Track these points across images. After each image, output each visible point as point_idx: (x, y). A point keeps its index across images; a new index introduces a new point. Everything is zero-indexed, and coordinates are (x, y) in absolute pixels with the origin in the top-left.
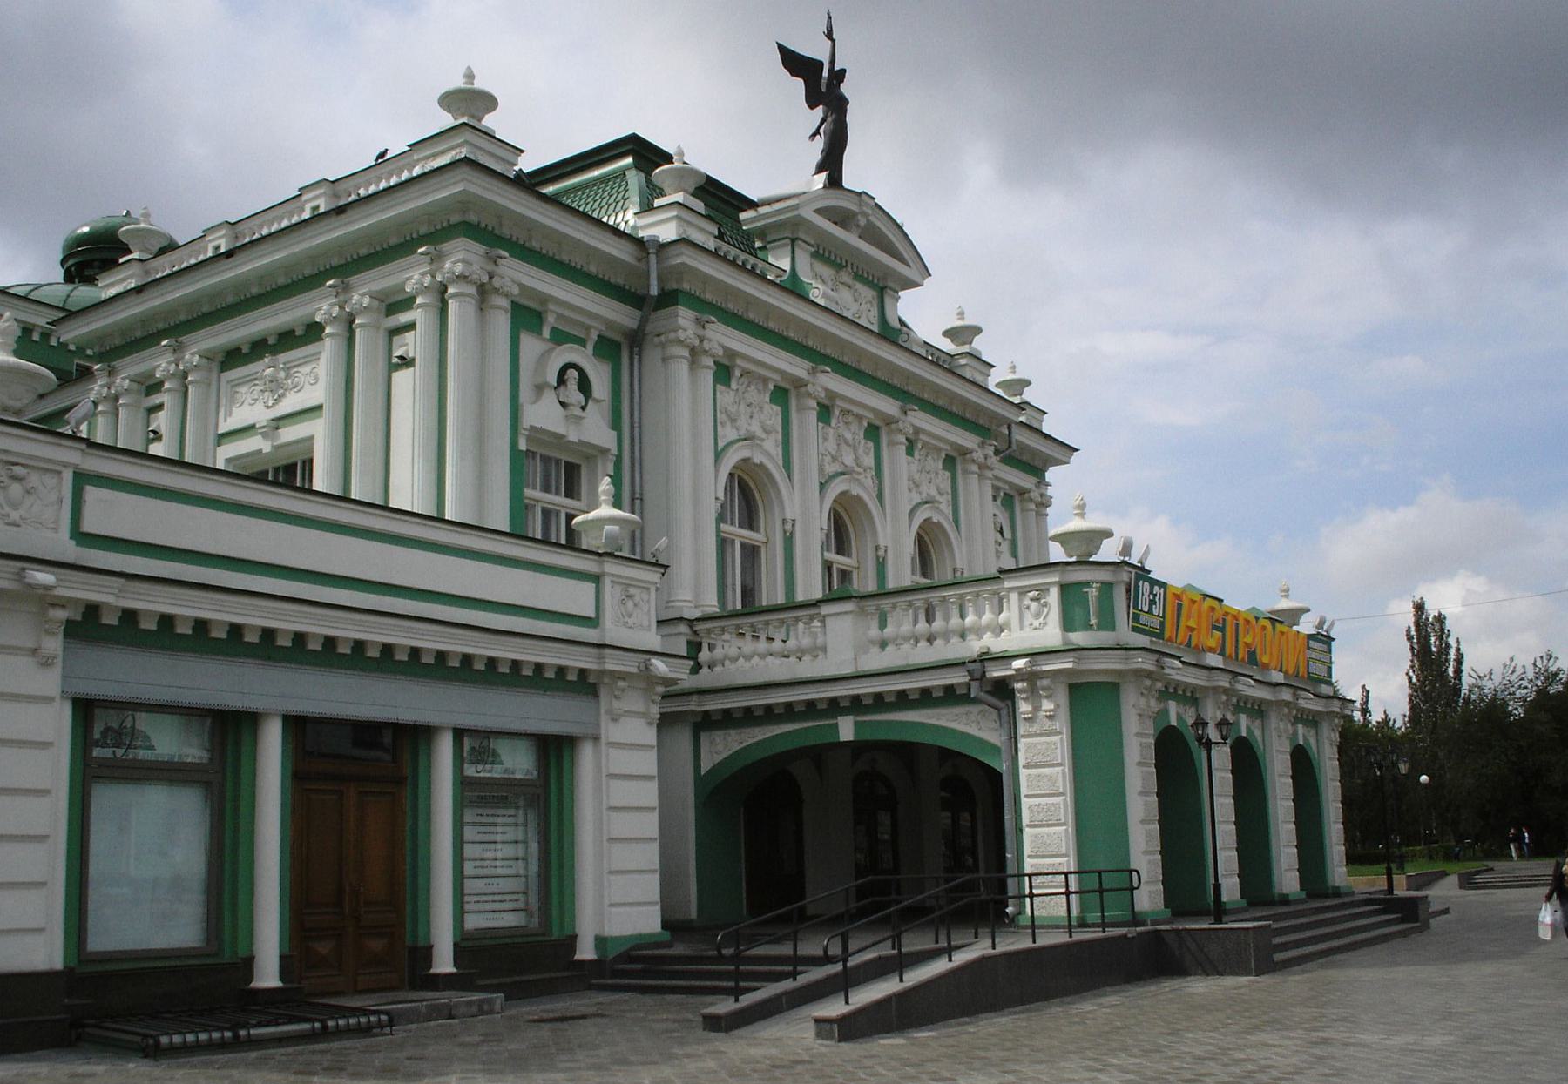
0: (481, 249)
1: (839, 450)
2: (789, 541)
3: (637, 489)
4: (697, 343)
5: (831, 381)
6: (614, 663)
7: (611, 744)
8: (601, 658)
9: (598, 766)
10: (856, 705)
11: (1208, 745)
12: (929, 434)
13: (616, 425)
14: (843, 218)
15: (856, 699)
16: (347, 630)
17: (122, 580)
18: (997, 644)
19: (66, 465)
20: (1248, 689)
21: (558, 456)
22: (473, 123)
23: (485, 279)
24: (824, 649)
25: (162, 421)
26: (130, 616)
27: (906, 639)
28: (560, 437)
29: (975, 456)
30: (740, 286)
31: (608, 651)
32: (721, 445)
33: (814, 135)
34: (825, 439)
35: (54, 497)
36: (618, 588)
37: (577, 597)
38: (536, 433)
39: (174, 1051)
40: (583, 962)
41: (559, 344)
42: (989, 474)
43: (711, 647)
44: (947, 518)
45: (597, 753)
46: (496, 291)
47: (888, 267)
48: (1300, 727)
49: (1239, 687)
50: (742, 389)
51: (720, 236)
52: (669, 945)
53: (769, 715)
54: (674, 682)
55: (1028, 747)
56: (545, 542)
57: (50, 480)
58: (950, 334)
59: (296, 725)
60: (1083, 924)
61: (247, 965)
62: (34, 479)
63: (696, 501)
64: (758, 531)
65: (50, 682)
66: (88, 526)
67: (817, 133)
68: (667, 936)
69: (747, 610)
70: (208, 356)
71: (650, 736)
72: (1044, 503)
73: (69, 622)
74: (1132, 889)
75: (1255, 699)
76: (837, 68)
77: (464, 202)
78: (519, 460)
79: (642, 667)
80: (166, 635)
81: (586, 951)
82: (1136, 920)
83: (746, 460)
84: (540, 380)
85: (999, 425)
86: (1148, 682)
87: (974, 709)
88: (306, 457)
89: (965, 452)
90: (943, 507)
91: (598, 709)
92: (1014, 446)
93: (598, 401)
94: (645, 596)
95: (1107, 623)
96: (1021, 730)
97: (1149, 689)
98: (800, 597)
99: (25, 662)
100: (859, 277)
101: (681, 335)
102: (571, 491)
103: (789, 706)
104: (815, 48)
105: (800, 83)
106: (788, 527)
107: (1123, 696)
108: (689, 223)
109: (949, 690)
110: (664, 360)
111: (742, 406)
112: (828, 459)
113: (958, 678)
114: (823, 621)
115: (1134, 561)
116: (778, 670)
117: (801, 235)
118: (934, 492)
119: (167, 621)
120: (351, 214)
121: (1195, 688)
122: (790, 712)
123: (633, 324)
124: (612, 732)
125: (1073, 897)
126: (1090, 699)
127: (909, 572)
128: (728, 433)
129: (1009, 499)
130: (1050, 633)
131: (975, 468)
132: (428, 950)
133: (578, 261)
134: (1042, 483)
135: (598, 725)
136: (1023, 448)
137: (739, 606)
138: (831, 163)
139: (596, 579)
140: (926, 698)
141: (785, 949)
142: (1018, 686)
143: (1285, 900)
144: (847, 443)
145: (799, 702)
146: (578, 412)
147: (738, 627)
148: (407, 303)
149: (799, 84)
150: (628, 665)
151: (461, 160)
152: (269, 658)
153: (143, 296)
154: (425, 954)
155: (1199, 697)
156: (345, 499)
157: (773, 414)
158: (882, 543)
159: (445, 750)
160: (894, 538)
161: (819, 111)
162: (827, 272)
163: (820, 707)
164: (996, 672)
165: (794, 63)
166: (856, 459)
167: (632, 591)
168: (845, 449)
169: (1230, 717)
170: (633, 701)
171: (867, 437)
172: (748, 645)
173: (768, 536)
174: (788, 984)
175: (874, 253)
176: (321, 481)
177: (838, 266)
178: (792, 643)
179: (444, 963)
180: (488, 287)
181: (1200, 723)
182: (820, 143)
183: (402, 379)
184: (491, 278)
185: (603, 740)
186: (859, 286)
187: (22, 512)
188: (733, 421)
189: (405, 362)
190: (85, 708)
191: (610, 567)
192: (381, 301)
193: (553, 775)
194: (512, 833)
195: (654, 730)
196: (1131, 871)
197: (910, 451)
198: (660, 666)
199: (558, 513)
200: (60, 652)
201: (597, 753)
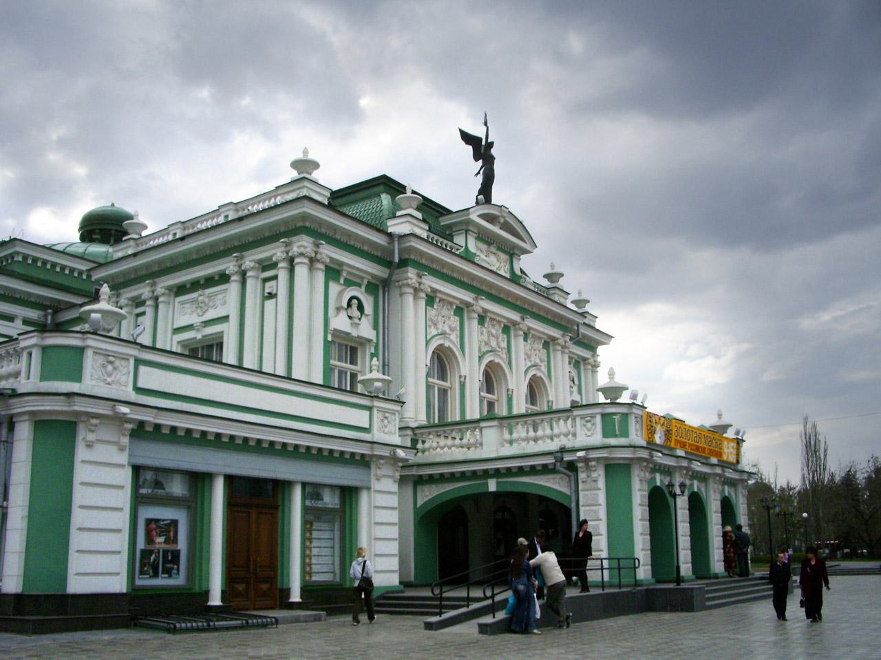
0: (311, 240)
2: (463, 386)
3: (386, 360)
4: (417, 286)
6: (378, 451)
7: (375, 491)
8: (372, 449)
9: (369, 503)
10: (497, 473)
11: (674, 496)
12: (535, 330)
13: (376, 327)
14: (490, 218)
15: (497, 470)
16: (212, 428)
17: (157, 411)
18: (568, 443)
19: (131, 356)
20: (697, 466)
21: (346, 343)
22: (307, 176)
23: (313, 255)
24: (481, 444)
25: (147, 321)
26: (158, 427)
28: (348, 334)
29: (559, 341)
31: (375, 445)
32: (429, 337)
33: (477, 174)
34: (482, 334)
35: (126, 370)
37: (360, 418)
38: (336, 333)
39: (182, 631)
41: (349, 287)
42: (567, 351)
43: (424, 442)
44: (544, 374)
45: (370, 498)
46: (318, 261)
47: (514, 243)
48: (726, 487)
49: (693, 466)
51: (430, 230)
52: (403, 592)
53: (453, 477)
54: (407, 460)
55: (584, 495)
56: (339, 389)
57: (124, 363)
58: (548, 276)
59: (230, 480)
60: (611, 586)
61: (206, 594)
62: (117, 363)
63: (416, 367)
65: (123, 458)
66: (140, 385)
67: (479, 173)
68: (402, 587)
69: (441, 424)
70: (169, 289)
71: (394, 487)
72: (595, 366)
73: (133, 430)
74: (635, 568)
75: (702, 473)
76: (489, 141)
78: (327, 345)
79: (392, 453)
80: (174, 436)
82: (637, 583)
83: (441, 345)
85: (572, 325)
86: (645, 464)
87: (558, 476)
88: (219, 341)
89: (554, 339)
90: (543, 368)
91: (370, 474)
92: (580, 337)
93: (367, 315)
94: (393, 417)
95: (625, 433)
96: (581, 487)
97: (645, 467)
98: (468, 417)
99: (114, 448)
100: (499, 249)
101: (409, 282)
102: (353, 362)
103: (463, 473)
104: (478, 131)
105: (470, 148)
106: (462, 379)
109: (545, 466)
111: (440, 317)
112: (483, 344)
113: (549, 460)
114: (481, 430)
115: (638, 402)
116: (458, 454)
117: (471, 228)
118: (538, 361)
119: (174, 429)
120: (245, 221)
121: (670, 467)
122: (463, 476)
124: (376, 485)
125: (604, 571)
126: (617, 470)
127: (524, 402)
128: (434, 332)
129: (577, 363)
130: (597, 438)
131: (559, 348)
133: (358, 245)
134: (595, 355)
135: (370, 481)
136: (585, 336)
137: (437, 421)
138: (486, 190)
139: (370, 409)
140: (533, 470)
141: (463, 594)
142: (580, 465)
143: (716, 576)
144: (493, 336)
145: (526, 466)
146: (357, 321)
147: (437, 432)
148: (274, 265)
149: (470, 149)
150: (385, 452)
151: (303, 197)
153: (138, 258)
154: (286, 592)
155: (676, 469)
156: (260, 372)
157: (455, 321)
158: (510, 387)
159: (297, 493)
160: (517, 384)
161: (480, 163)
162: (483, 246)
163: (525, 470)
164: (567, 458)
165: (467, 138)
166: (498, 343)
167: (387, 415)
168: (492, 338)
169: (688, 482)
170: (386, 470)
171: (503, 332)
172: (442, 442)
173: (453, 383)
174: (464, 610)
176: (230, 356)
177: (489, 244)
178: (465, 441)
179: (296, 597)
180: (314, 259)
181: (671, 485)
182: (480, 178)
183: (269, 304)
185: (372, 490)
186: (500, 253)
187: (113, 378)
188: (435, 325)
189: (271, 296)
190: (137, 470)
191: (377, 403)
192: (259, 264)
193: (348, 507)
194: (326, 535)
196: (634, 559)
197: (525, 340)
198: (401, 453)
199: (346, 372)
200: (128, 444)
201: (370, 498)
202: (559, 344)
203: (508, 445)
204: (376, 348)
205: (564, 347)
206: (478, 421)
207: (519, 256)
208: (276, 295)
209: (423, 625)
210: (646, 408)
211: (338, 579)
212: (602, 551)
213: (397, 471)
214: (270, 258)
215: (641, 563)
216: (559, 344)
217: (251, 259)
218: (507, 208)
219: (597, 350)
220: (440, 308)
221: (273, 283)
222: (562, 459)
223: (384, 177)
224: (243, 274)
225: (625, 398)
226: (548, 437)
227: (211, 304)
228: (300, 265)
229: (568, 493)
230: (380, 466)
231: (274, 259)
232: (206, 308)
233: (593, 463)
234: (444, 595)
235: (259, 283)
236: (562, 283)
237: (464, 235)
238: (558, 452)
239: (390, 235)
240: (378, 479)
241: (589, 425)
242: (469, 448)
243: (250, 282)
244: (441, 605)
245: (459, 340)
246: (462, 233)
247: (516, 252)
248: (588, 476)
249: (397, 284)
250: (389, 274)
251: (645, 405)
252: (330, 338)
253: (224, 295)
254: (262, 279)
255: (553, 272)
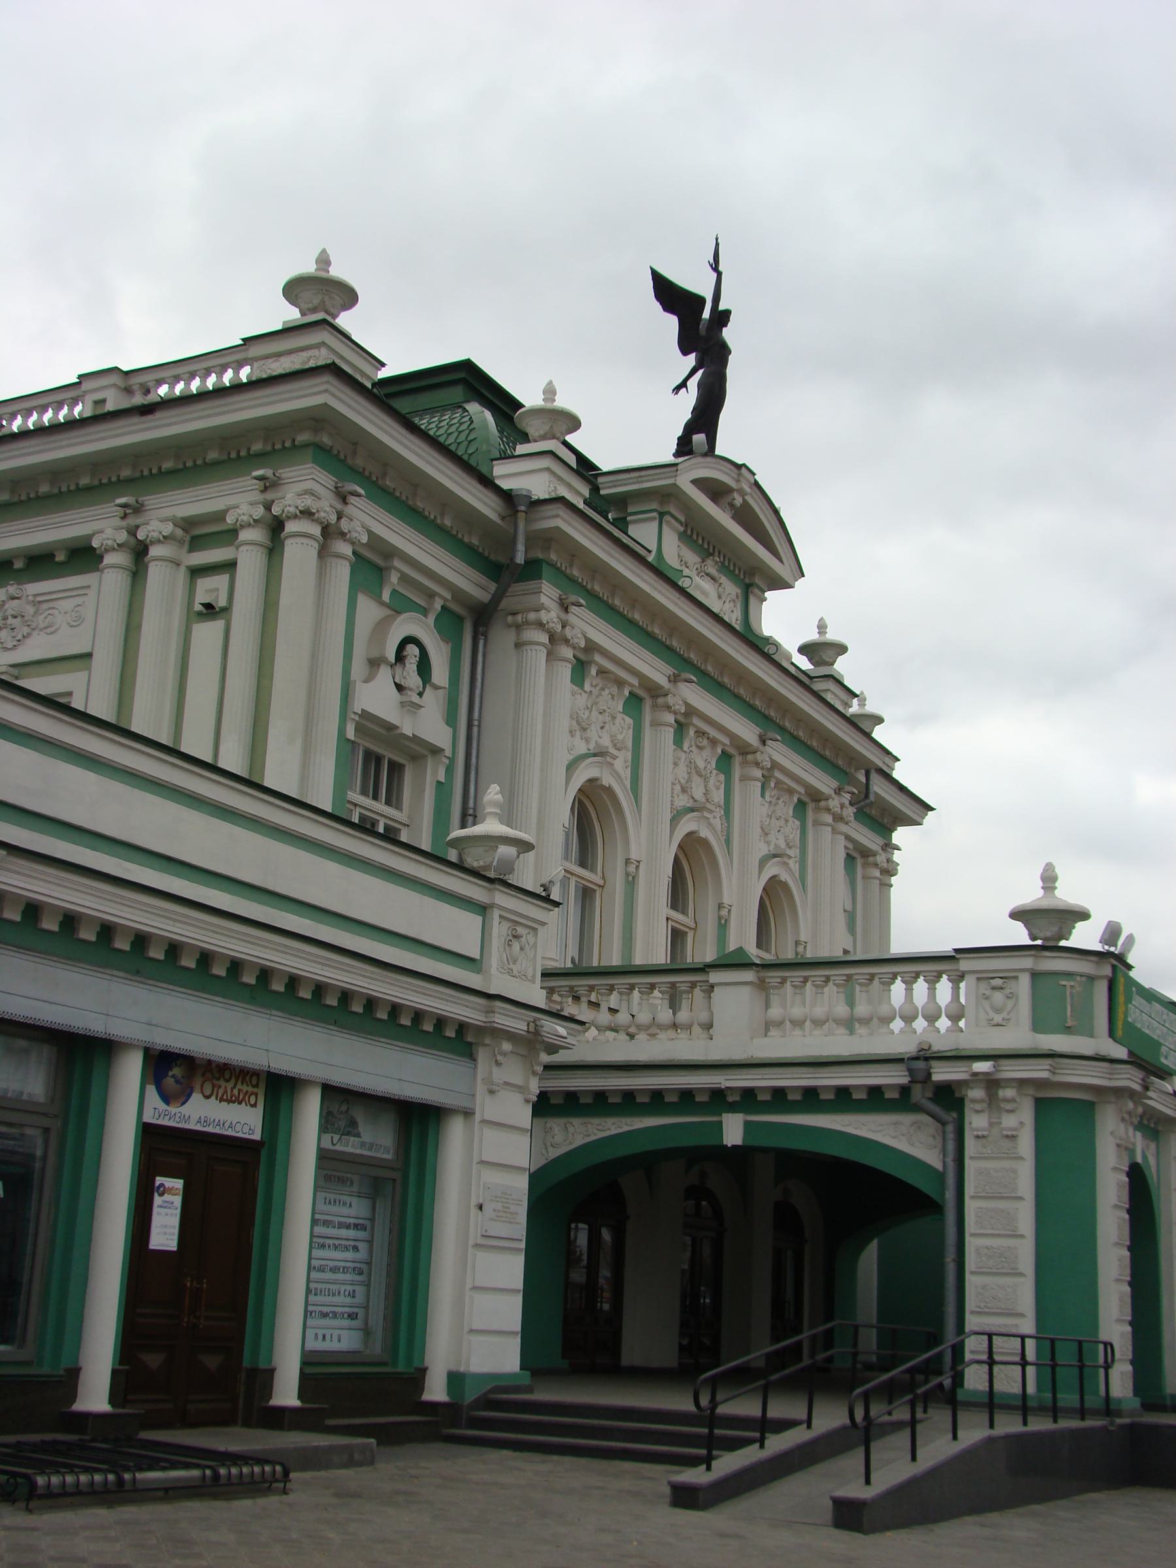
1: (689, 780)
2: (631, 882)
3: (471, 804)
5: (693, 695)
8: (489, 1011)
10: (748, 1099)
13: (451, 719)
14: (716, 491)
22: (329, 318)
27: (663, 1027)
28: (391, 727)
30: (614, 564)
31: (498, 1004)
33: (677, 389)
36: (506, 925)
38: (369, 723)
40: (86, 1416)
42: (843, 828)
46: (343, 535)
50: (596, 691)
52: (529, 1389)
53: (629, 1102)
61: (70, 1380)
64: (593, 870)
67: (683, 384)
68: (526, 1378)
71: (523, 1115)
76: (722, 307)
77: (320, 419)
81: (436, 1391)
84: (375, 654)
85: (857, 770)
87: (907, 1119)
90: (791, 862)
92: (872, 797)
93: (436, 688)
98: (638, 960)
100: (725, 569)
101: (544, 616)
104: (699, 283)
107: (1098, 1117)
108: (560, 479)
110: (518, 645)
111: (595, 713)
112: (678, 788)
113: (893, 1077)
122: (657, 1101)
123: (484, 596)
124: (487, 1107)
126: (1063, 1117)
129: (857, 856)
131: (828, 819)
132: (73, 1375)
138: (706, 417)
139: (483, 909)
140: (844, 1100)
146: (415, 699)
149: (672, 323)
150: (517, 1023)
152: (138, 973)
154: (265, 1378)
157: (623, 727)
160: (738, 890)
163: (823, 1096)
164: (942, 1073)
165: (669, 294)
167: (520, 930)
168: (695, 778)
170: (512, 1071)
175: (745, 539)
179: (286, 1394)
183: (208, 633)
184: (339, 518)
185: (478, 1117)
186: (723, 580)
191: (503, 899)
195: (528, 1110)
202: (828, 810)
203: (842, 1030)
204: (450, 770)
205: (838, 818)
206: (705, 968)
207: (764, 592)
208: (226, 610)
209: (667, 1490)
210: (1130, 967)
211: (377, 1348)
212: (1022, 1315)
213: (534, 1073)
214: (220, 516)
215: (1117, 1356)
216: (828, 810)
217: (166, 510)
218: (754, 474)
219: (894, 835)
220: (596, 691)
221: (220, 581)
222: (929, 1075)
223: (467, 366)
224: (140, 552)
225: (1085, 936)
226: (838, 1022)
227: (41, 621)
228: (300, 540)
229: (938, 1166)
230: (499, 1058)
231: (230, 519)
232: (26, 630)
233: (1009, 1093)
234: (722, 1410)
235: (182, 575)
236: (842, 666)
237: (656, 524)
238: (917, 1058)
239: (508, 497)
240: (492, 1092)
241: (998, 997)
242: (632, 1036)
243: (156, 573)
244: (714, 1435)
245: (629, 771)
246: (653, 519)
247: (757, 581)
248: (991, 1124)
249: (510, 619)
250: (494, 596)
251: (1130, 961)
252: (351, 734)
253: (79, 600)
254: (188, 567)
255: (822, 639)
